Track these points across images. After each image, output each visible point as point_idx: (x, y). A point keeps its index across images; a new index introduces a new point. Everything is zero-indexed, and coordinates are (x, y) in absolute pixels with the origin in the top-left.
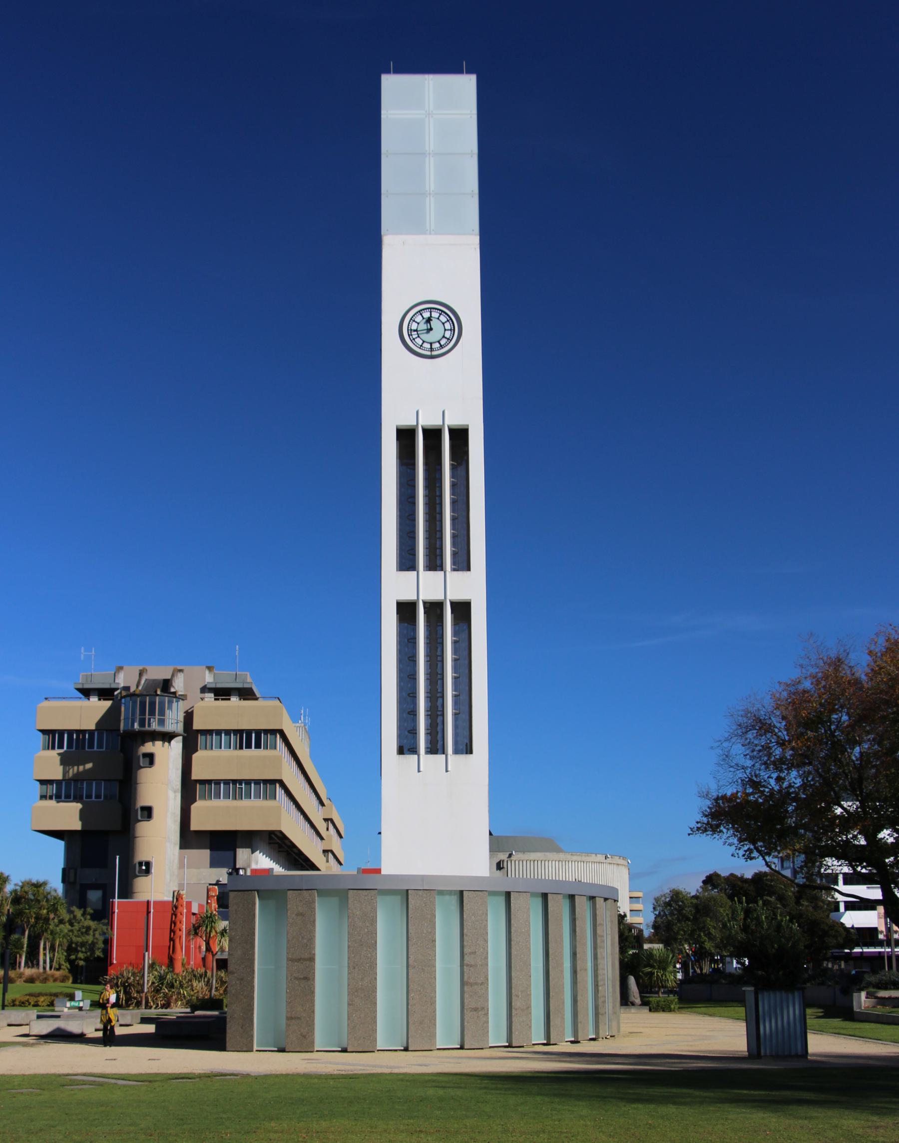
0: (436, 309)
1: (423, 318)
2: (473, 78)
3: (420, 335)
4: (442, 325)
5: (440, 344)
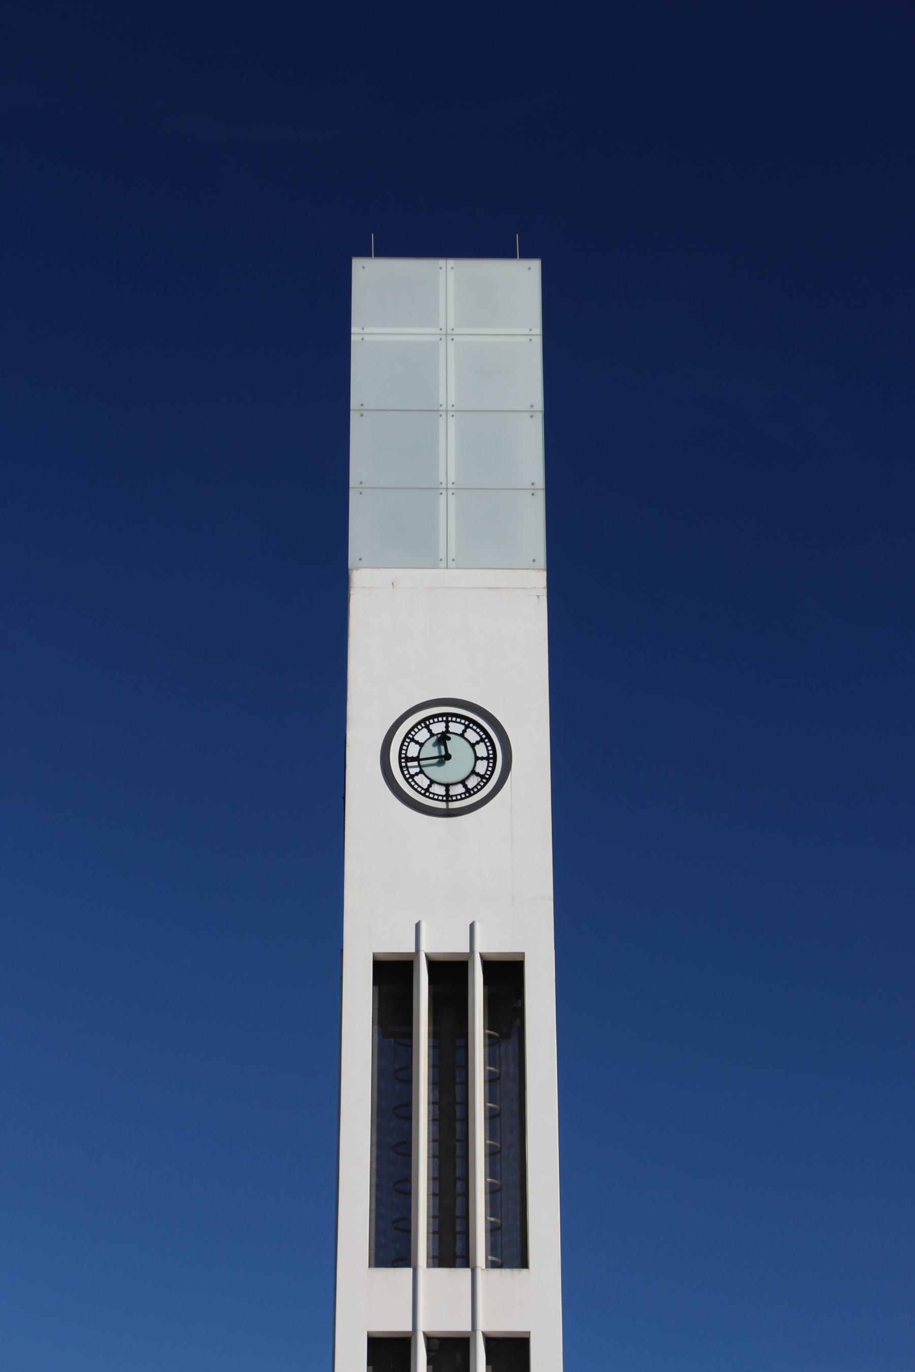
1: (432, 735)
3: (423, 769)
4: (470, 749)
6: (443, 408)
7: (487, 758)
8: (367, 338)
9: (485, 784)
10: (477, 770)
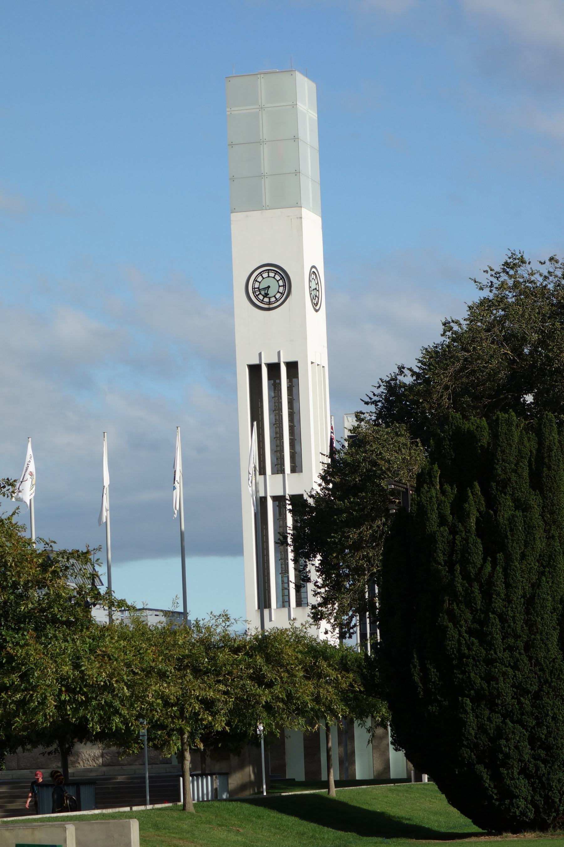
2: (304, 780)
5: (276, 298)
6: (263, 175)
7: (283, 286)
8: (232, 112)
9: (283, 296)
10: (280, 285)
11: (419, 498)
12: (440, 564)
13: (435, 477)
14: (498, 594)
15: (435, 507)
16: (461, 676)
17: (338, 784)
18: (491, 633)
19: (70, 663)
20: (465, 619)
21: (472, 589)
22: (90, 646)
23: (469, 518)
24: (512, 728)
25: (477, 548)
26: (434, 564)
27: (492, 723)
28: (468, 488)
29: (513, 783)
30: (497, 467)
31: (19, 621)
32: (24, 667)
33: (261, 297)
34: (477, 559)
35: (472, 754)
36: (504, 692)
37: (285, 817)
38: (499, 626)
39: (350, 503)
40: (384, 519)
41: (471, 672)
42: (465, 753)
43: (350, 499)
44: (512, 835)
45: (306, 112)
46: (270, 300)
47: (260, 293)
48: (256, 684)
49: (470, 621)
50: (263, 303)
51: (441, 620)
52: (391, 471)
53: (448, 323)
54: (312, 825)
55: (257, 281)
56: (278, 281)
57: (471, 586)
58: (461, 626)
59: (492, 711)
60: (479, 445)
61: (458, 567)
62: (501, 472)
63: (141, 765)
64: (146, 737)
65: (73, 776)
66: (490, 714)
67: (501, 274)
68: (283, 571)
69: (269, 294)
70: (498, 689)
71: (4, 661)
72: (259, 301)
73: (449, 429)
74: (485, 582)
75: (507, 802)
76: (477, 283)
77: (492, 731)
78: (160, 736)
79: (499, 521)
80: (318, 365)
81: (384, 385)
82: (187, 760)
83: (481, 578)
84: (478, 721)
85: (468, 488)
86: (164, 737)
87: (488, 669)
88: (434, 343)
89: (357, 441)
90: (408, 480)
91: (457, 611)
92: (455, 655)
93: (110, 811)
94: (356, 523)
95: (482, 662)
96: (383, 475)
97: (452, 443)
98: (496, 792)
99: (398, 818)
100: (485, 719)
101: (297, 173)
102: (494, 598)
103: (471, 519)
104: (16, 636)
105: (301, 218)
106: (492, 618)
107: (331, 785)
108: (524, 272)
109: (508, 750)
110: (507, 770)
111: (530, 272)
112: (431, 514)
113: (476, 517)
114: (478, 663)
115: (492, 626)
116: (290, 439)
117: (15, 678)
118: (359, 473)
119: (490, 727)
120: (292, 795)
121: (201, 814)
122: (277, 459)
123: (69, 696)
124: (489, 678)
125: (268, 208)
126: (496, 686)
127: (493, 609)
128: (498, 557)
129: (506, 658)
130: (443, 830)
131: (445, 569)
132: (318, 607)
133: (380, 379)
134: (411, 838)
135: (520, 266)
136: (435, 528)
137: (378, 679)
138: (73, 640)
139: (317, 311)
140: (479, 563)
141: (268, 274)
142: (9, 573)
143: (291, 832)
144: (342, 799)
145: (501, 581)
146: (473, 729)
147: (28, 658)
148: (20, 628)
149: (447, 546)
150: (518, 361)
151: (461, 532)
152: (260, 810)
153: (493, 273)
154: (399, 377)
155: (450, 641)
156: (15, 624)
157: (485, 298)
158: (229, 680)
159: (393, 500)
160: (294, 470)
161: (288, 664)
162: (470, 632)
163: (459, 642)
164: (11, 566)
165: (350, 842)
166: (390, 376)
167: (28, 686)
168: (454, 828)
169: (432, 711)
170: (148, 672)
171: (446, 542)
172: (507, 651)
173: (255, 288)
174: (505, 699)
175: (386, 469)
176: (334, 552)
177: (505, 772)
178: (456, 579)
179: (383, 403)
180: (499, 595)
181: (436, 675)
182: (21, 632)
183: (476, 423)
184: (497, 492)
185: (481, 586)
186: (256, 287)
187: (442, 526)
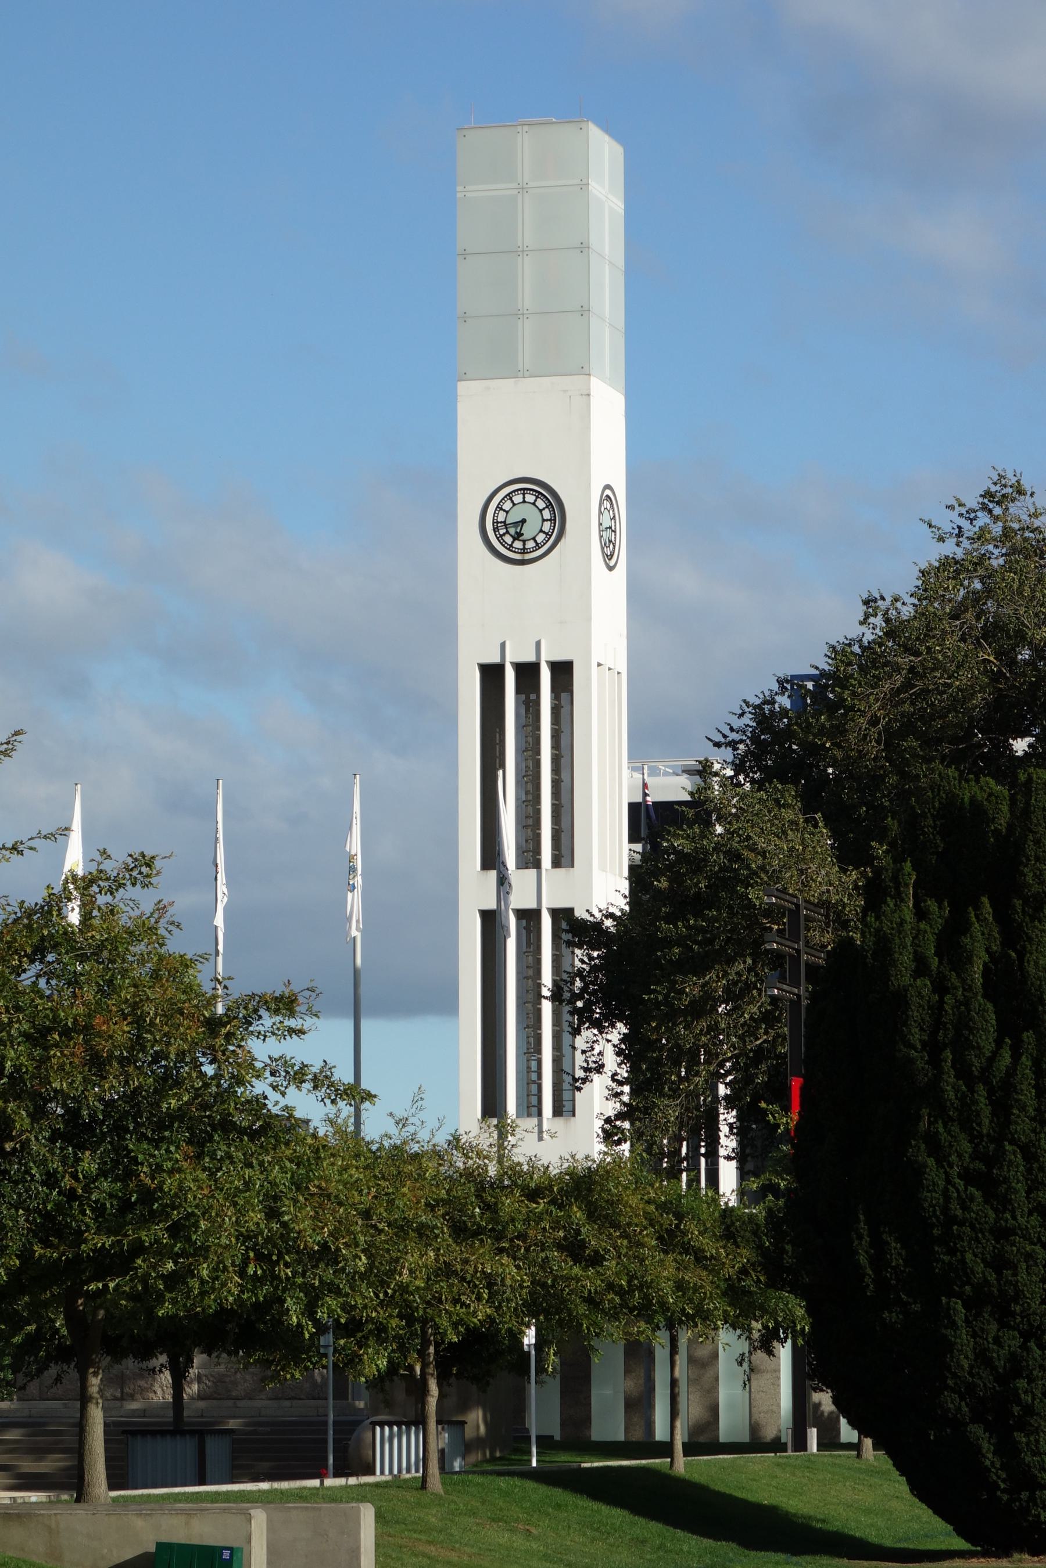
0: (531, 490)
4: (539, 513)
5: (536, 541)
6: (520, 312)
7: (550, 520)
8: (468, 195)
9: (549, 539)
10: (545, 518)
11: (877, 923)
12: (914, 1047)
13: (907, 885)
14: (1023, 1108)
15: (908, 941)
16: (946, 1258)
17: (689, 1449)
18: (1006, 1180)
19: (260, 1207)
20: (957, 1152)
21: (973, 1095)
22: (292, 1177)
23: (971, 964)
24: (1039, 1359)
25: (986, 1021)
26: (902, 1047)
27: (1002, 1347)
28: (970, 908)
29: (1038, 1461)
30: (1026, 870)
31: (160, 1126)
32: (175, 1212)
33: (508, 539)
34: (986, 1038)
35: (963, 1403)
36: (1028, 1291)
37: (605, 1509)
38: (1021, 1168)
39: (689, 928)
40: (749, 961)
41: (966, 1251)
42: (949, 1401)
43: (688, 921)
44: (1030, 1558)
45: (604, 199)
46: (524, 545)
47: (507, 532)
48: (569, 1259)
49: (967, 1156)
50: (512, 551)
51: (913, 1152)
52: (767, 872)
53: (872, 601)
54: (655, 1527)
55: (501, 509)
56: (541, 511)
57: (972, 1090)
58: (951, 1166)
59: (1003, 1325)
60: (993, 828)
61: (948, 1055)
62: (1033, 880)
63: (270, 1399)
64: (331, 1349)
65: (144, 1417)
66: (999, 1330)
67: (979, 514)
68: (531, 1047)
69: (523, 534)
70: (1016, 1286)
71: (133, 1199)
72: (504, 546)
73: (934, 798)
74: (1000, 1084)
75: (1024, 1495)
76: (933, 529)
77: (1002, 1362)
78: (343, 1348)
79: (1028, 972)
80: (610, 669)
81: (750, 712)
82: (433, 1396)
83: (991, 1077)
84: (976, 1343)
85: (970, 908)
86: (350, 1349)
87: (998, 1246)
88: (846, 638)
89: (702, 812)
90: (799, 890)
91: (944, 1136)
92: (938, 1218)
93: (285, 1485)
94: (697, 965)
95: (987, 1234)
96: (753, 879)
97: (938, 823)
98: (1004, 1476)
99: (803, 1517)
100: (990, 1340)
101: (584, 311)
102: (1014, 1114)
103: (976, 966)
104: (156, 1152)
105: (589, 395)
106: (1009, 1152)
107: (676, 1451)
108: (1021, 511)
109: (1030, 1399)
110: (1027, 1436)
111: (1033, 510)
112: (901, 954)
113: (984, 962)
114: (980, 1235)
115: (1008, 1168)
116: (553, 805)
117: (159, 1230)
118: (706, 873)
119: (999, 1356)
120: (597, 1468)
121: (455, 1498)
122: (527, 841)
123: (261, 1268)
124: (999, 1263)
125: (527, 374)
126: (1012, 1279)
127: (1013, 1135)
128: (1026, 1040)
129: (1033, 1227)
130: (888, 1543)
131: (922, 1058)
132: (616, 1120)
133: (745, 701)
134: (840, 1555)
135: (1013, 500)
136: (907, 980)
137: (790, 1258)
138: (261, 1164)
139: (611, 569)
140: (988, 1048)
141: (524, 498)
142: (149, 1036)
143: (620, 1537)
144: (697, 1477)
145: (1030, 1084)
146: (967, 1357)
147: (183, 1195)
148: (162, 1139)
149: (928, 1013)
150: (1008, 675)
151: (956, 988)
152: (558, 1494)
153: (963, 510)
154: (778, 698)
155: (929, 1191)
156: (154, 1131)
157: (947, 557)
158: (520, 1249)
159: (768, 925)
160: (556, 863)
161: (629, 1224)
162: (967, 1176)
163: (945, 1193)
164: (152, 1023)
165: (731, 1561)
166: (761, 696)
167: (187, 1246)
168: (907, 1539)
169: (891, 1320)
170: (401, 1228)
171: (926, 1008)
172: (1036, 1214)
173: (498, 522)
174: (1029, 1304)
175: (758, 867)
176: (653, 1019)
177: (1024, 1439)
178: (945, 1077)
179: (747, 745)
180: (1024, 1110)
181: (899, 1254)
182: (165, 1147)
183: (989, 787)
184: (1025, 918)
185: (991, 1092)
186: (499, 520)
187: (919, 978)
